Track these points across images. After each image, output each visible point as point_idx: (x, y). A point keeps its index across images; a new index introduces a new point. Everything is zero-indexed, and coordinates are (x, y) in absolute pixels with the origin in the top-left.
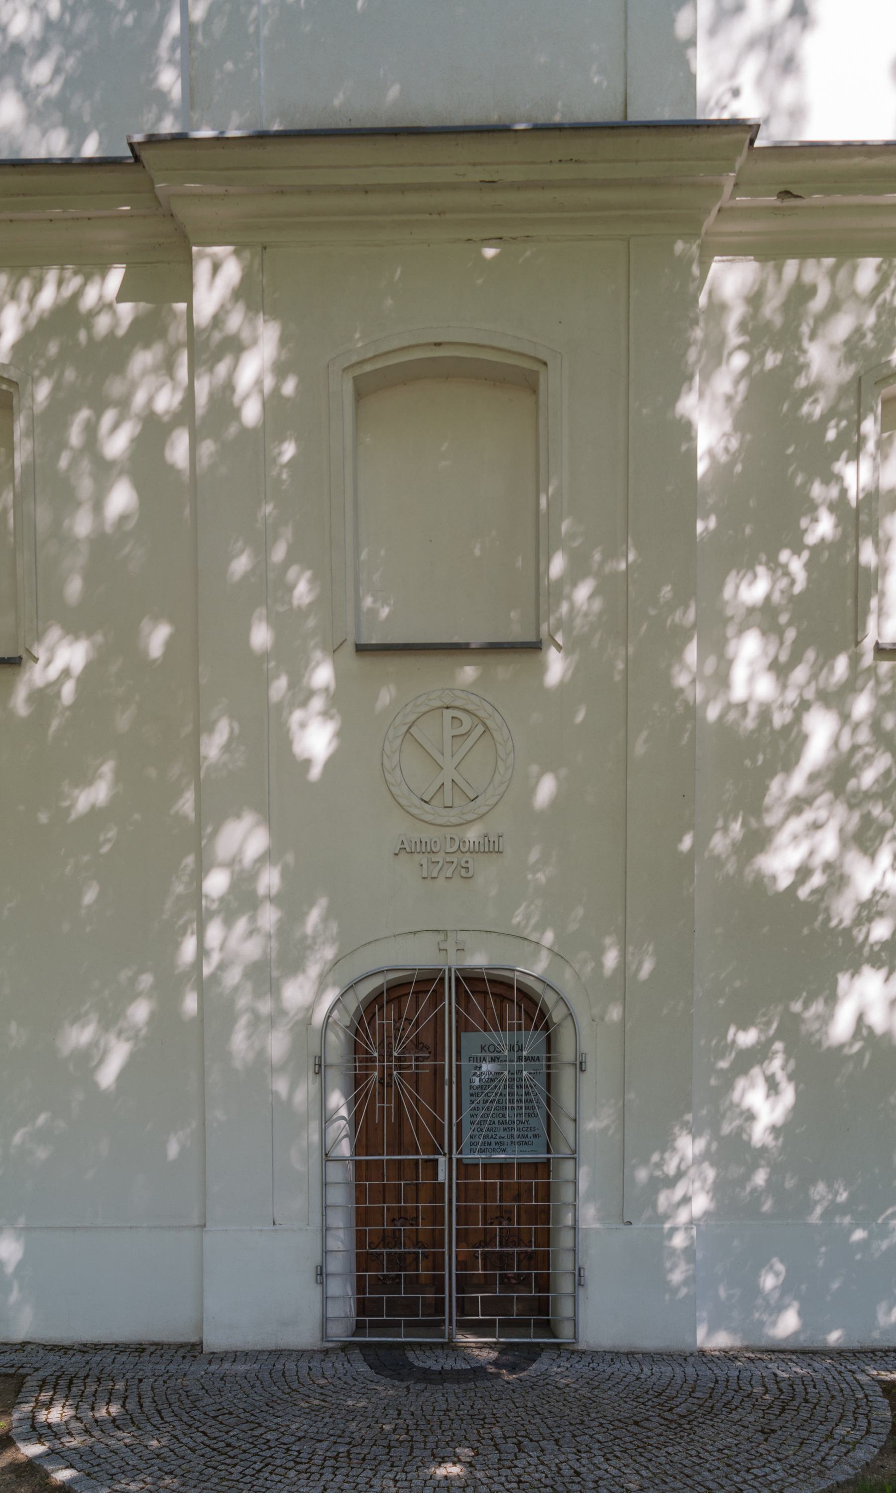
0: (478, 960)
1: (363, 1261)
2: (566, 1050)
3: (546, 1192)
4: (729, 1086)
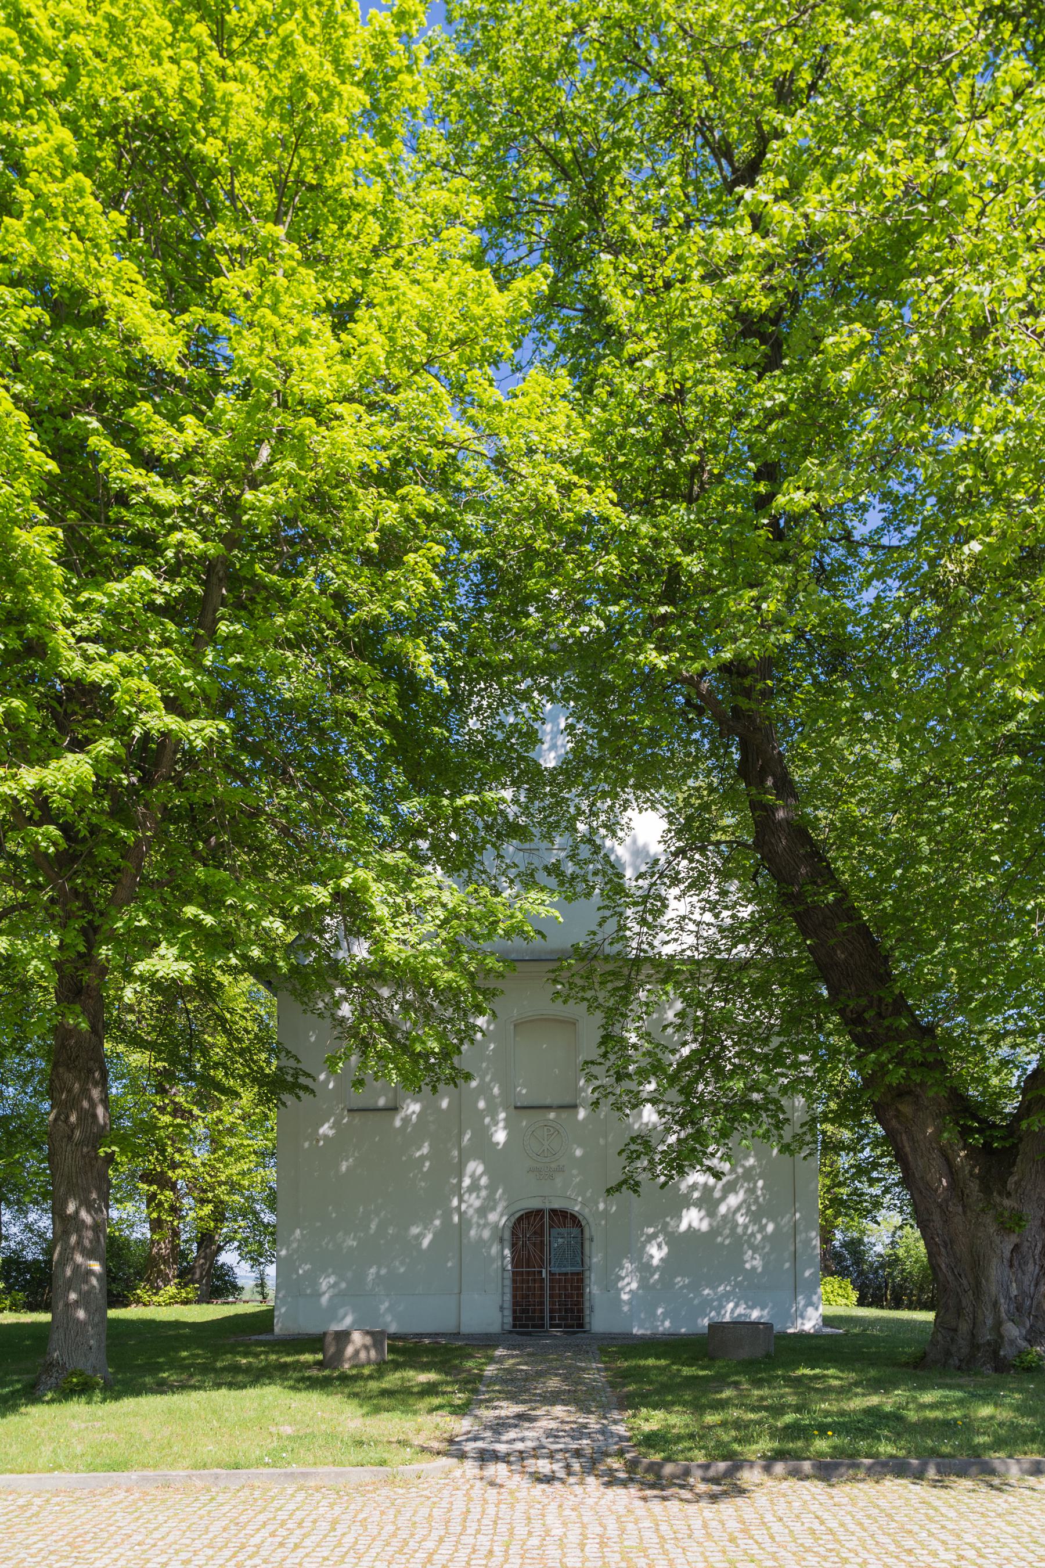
0: (556, 1206)
1: (515, 1303)
2: (587, 1235)
3: (582, 1281)
4: (644, 1247)
